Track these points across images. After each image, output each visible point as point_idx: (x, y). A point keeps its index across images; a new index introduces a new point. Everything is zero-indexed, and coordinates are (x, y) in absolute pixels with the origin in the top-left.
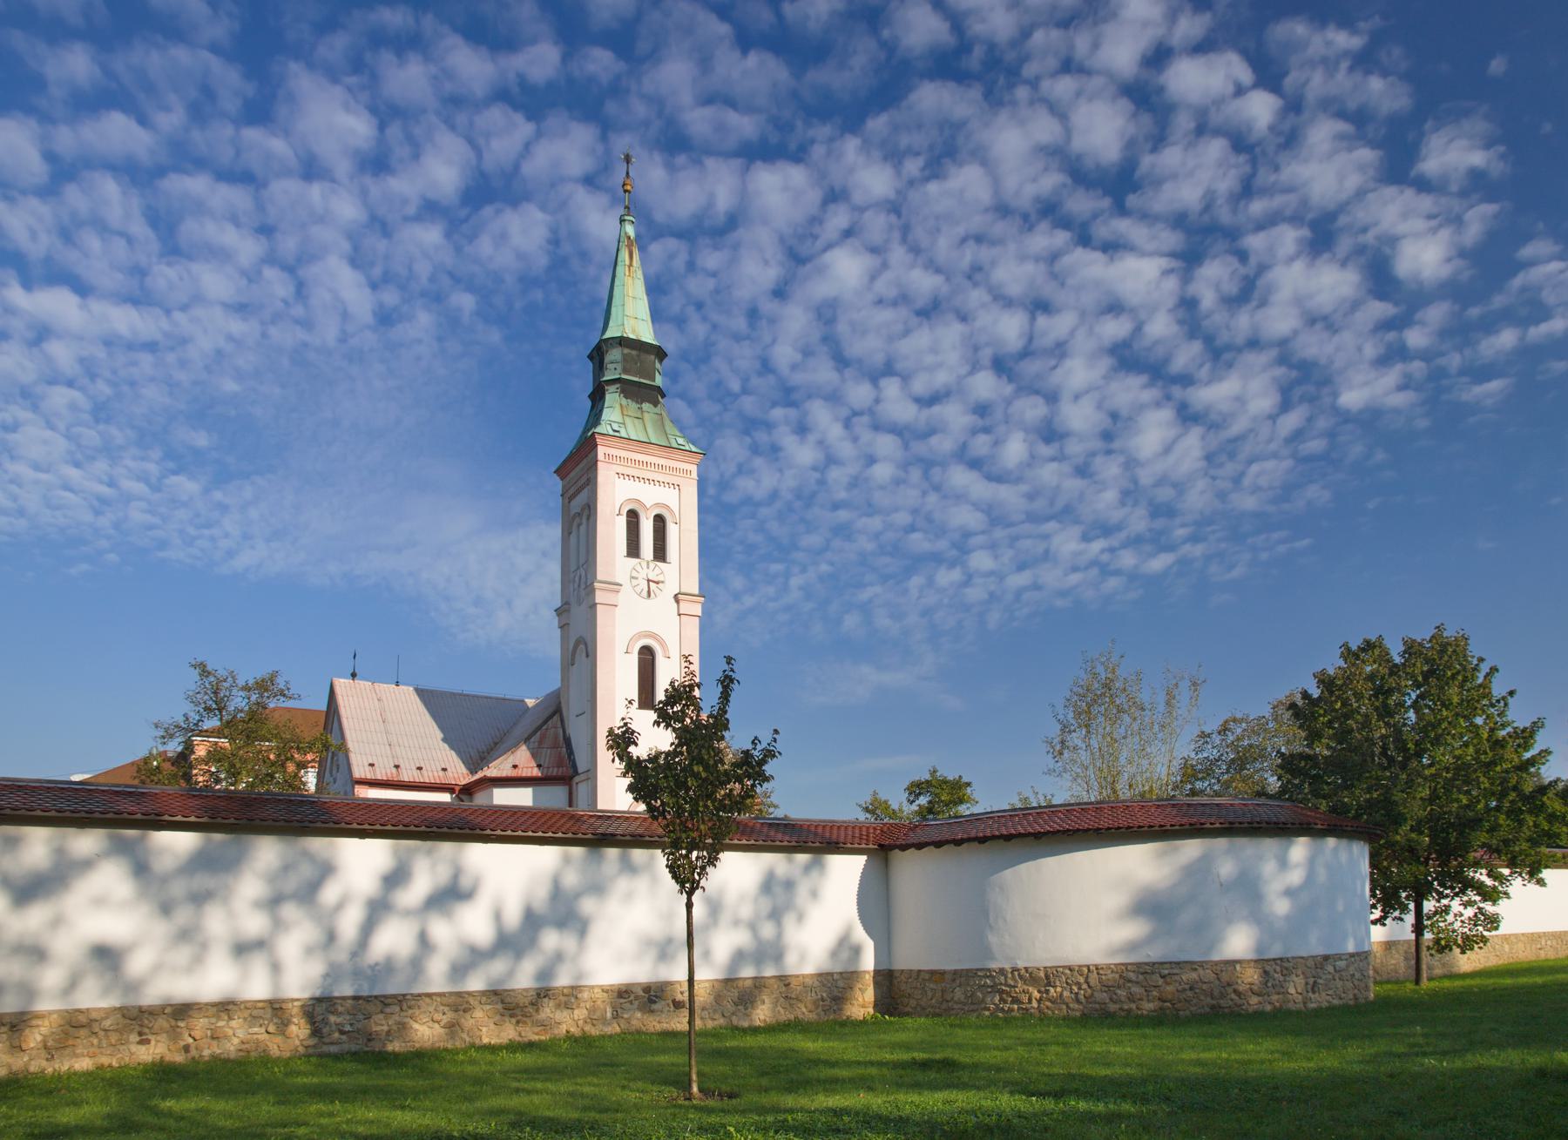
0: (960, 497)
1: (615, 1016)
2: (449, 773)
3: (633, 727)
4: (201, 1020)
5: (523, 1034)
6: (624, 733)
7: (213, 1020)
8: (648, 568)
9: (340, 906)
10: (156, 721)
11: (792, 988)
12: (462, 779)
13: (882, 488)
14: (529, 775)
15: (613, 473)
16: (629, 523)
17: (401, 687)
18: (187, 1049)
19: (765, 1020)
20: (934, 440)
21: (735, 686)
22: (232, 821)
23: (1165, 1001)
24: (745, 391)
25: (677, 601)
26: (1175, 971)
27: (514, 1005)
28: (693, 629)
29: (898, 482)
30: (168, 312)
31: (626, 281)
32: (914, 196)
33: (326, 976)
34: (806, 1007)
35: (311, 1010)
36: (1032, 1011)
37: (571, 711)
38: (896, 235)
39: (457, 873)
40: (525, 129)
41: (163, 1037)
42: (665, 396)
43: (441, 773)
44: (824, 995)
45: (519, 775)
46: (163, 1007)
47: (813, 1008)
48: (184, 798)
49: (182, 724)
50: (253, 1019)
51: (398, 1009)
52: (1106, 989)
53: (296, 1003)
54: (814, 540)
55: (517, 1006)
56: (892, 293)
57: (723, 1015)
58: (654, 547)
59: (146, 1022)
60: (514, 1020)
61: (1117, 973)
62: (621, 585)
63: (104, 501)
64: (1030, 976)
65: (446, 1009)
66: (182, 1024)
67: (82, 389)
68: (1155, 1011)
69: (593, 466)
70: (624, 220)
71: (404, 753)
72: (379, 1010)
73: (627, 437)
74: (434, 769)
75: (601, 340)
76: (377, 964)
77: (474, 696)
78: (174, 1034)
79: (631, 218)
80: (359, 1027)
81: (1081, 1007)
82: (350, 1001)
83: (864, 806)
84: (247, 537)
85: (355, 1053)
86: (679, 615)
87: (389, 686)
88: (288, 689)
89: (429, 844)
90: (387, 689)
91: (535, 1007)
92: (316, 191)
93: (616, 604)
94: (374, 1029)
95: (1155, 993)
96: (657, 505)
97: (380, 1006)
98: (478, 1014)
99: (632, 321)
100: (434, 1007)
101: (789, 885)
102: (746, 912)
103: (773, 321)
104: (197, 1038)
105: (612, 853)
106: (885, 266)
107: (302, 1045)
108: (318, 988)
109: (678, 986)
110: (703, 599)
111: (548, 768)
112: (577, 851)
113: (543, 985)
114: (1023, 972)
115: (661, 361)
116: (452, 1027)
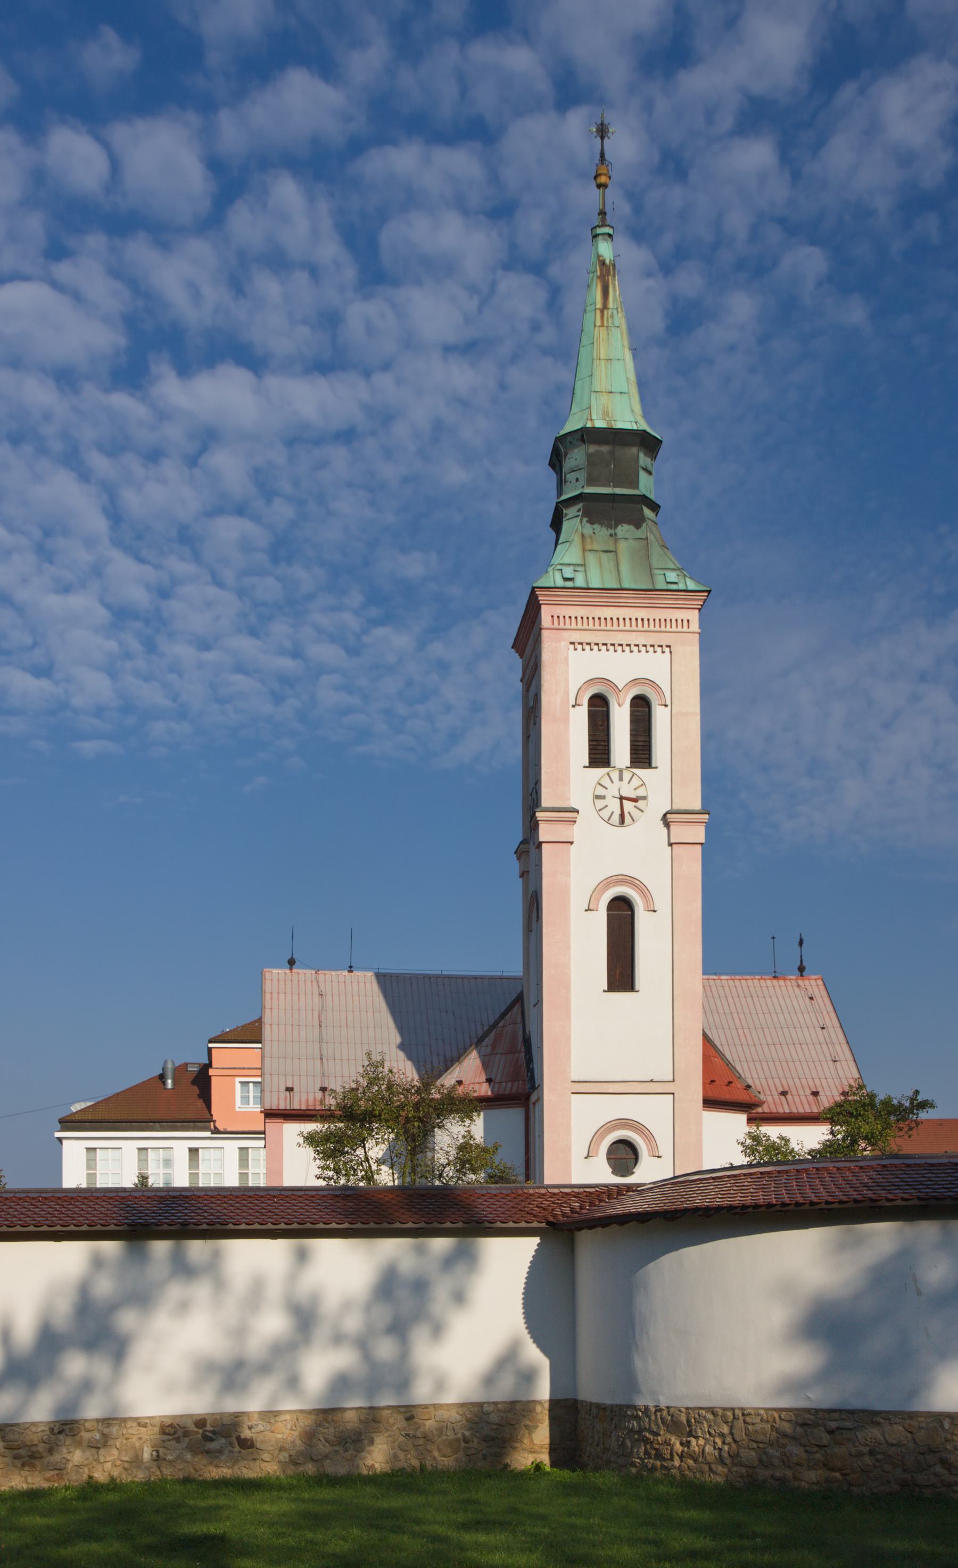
8: (621, 779)
11: (416, 1423)
16: (592, 717)
17: (356, 973)
23: (833, 1470)
25: (667, 824)
26: (848, 1424)
30: (367, 374)
36: (673, 1471)
42: (659, 507)
47: (449, 1452)
52: (755, 1445)
61: (768, 1421)
63: (287, 681)
64: (672, 1420)
67: (257, 519)
68: (818, 1483)
81: (726, 1470)
86: (671, 845)
90: (335, 979)
91: (47, 1446)
95: (818, 1456)
96: (635, 682)
101: (420, 1286)
102: (353, 1323)
105: (161, 1248)
110: (707, 816)
111: (500, 1083)
112: (110, 1248)
113: (70, 1417)
114: (665, 1413)
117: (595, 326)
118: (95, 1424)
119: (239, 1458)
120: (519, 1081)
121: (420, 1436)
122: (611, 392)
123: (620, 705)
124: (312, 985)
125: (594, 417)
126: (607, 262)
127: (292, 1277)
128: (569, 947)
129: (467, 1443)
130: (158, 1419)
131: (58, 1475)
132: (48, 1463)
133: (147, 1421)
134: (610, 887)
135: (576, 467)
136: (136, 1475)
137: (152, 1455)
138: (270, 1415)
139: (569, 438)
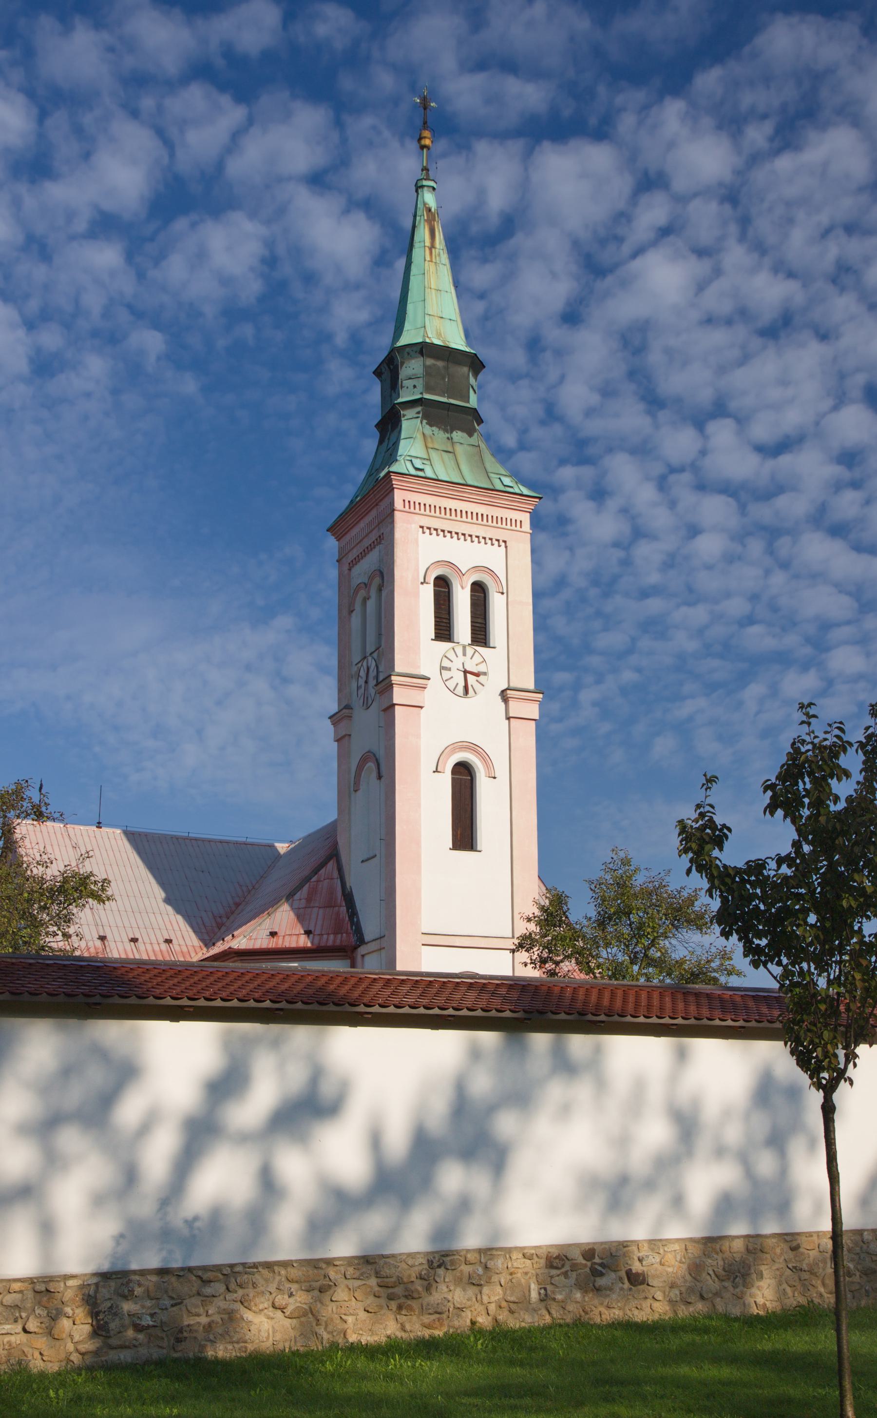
0: (816, 577)
1: (543, 1296)
2: (175, 946)
3: (719, 820)
8: (464, 654)
9: (145, 1129)
11: (802, 1254)
12: (193, 954)
13: (709, 567)
15: (415, 527)
17: (104, 829)
19: (765, 1305)
20: (782, 502)
27: (393, 1280)
29: (730, 559)
31: (427, 268)
32: (760, 176)
34: (824, 1285)
35: (92, 1293)
38: (733, 229)
39: (317, 1074)
43: (164, 946)
45: (280, 946)
53: (70, 1283)
54: (614, 639)
56: (726, 307)
57: (702, 1297)
58: (472, 626)
60: (394, 1305)
62: (429, 679)
65: (294, 1287)
69: (388, 516)
70: (422, 187)
72: (194, 1290)
73: (434, 477)
74: (154, 941)
76: (196, 1218)
79: (432, 184)
80: (164, 1319)
82: (154, 1278)
85: (160, 1363)
87: (87, 828)
88: (47, 804)
89: (275, 1028)
91: (425, 1283)
94: (186, 1323)
97: (197, 1283)
98: (341, 1294)
99: (436, 322)
100: (275, 1285)
102: (733, 1134)
103: (560, 353)
105: (541, 1041)
106: (718, 272)
107: (77, 1350)
109: (634, 1248)
110: (541, 696)
112: (489, 1038)
113: (445, 1247)
115: (476, 375)
117: (425, 260)
118: (477, 1255)
119: (630, 1297)
120: (342, 934)
121: (806, 1269)
123: (463, 588)
124: (63, 837)
126: (433, 210)
128: (419, 805)
130: (545, 1248)
131: (439, 1319)
132: (428, 1305)
133: (533, 1251)
134: (456, 752)
136: (524, 1319)
137: (540, 1294)
138: (654, 1243)
139: (407, 350)
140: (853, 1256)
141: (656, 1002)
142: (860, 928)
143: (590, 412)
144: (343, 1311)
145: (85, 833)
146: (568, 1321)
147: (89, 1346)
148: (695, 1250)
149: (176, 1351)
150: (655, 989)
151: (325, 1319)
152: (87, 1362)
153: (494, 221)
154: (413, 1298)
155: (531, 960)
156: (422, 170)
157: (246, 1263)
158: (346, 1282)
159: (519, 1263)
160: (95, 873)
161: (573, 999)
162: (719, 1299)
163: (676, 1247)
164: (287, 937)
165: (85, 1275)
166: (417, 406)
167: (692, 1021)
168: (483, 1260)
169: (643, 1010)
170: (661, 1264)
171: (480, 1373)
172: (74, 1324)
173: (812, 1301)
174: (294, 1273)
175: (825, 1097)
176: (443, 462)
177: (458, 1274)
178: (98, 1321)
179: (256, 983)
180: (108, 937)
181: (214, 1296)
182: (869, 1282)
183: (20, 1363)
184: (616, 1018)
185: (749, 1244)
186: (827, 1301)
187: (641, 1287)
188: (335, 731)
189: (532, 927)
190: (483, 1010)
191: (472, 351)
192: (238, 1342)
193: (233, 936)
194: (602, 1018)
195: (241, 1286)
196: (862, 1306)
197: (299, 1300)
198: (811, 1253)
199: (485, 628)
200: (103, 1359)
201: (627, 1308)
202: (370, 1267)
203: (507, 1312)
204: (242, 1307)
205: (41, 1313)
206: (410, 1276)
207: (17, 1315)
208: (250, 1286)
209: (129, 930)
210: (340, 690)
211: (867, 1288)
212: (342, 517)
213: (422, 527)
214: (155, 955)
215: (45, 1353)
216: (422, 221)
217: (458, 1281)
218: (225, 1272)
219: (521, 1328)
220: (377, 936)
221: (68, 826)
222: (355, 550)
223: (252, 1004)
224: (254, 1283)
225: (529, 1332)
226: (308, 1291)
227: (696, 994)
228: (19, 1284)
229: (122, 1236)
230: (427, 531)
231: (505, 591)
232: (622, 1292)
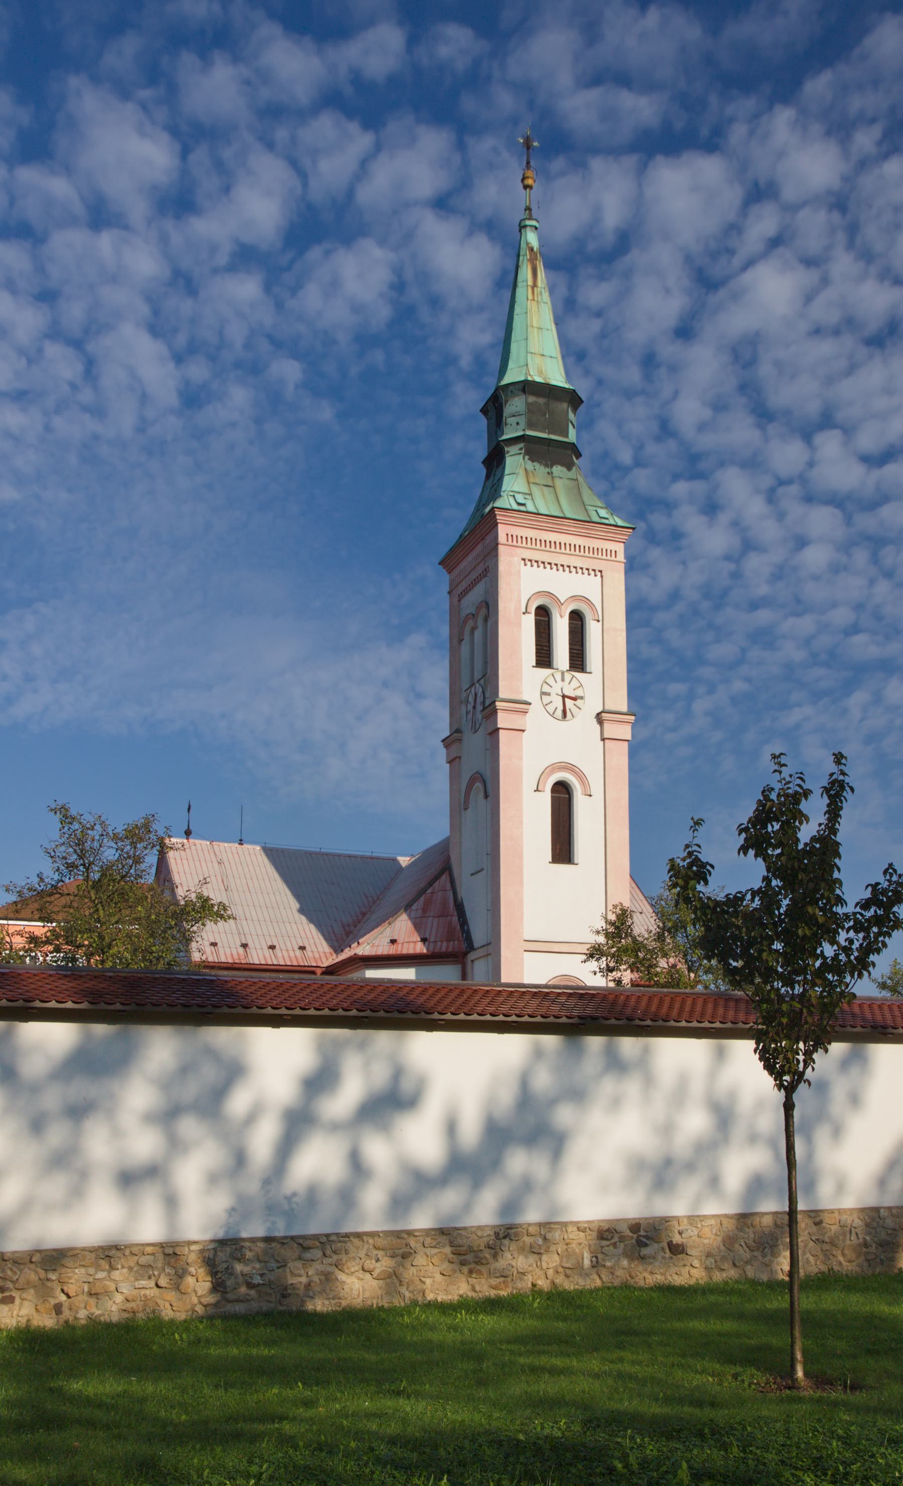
1: (594, 1263)
2: (308, 953)
3: (703, 858)
4: (77, 1271)
5: (478, 1288)
6: (691, 865)
7: (91, 1271)
8: (563, 680)
9: (252, 1118)
10: (7, 883)
11: (825, 1228)
12: (324, 960)
13: (816, 578)
14: (411, 951)
15: (517, 560)
16: (538, 624)
17: (246, 846)
18: (58, 1309)
20: (886, 512)
21: (847, 794)
22: (118, 1006)
24: (638, 463)
27: (464, 1248)
28: (620, 757)
29: (836, 569)
32: (867, 182)
33: (232, 1211)
34: (843, 1255)
35: (211, 1256)
37: (463, 869)
38: (841, 237)
39: (398, 1073)
40: (363, 141)
41: (30, 1294)
42: (581, 455)
43: (298, 953)
44: (868, 1238)
45: (399, 952)
46: (31, 1254)
48: (53, 979)
49: (37, 886)
50: (145, 1270)
51: (320, 1254)
53: (193, 1247)
54: (724, 651)
55: (470, 1250)
56: (833, 317)
57: (734, 1265)
58: (570, 653)
59: (9, 1273)
60: (465, 1270)
62: (530, 704)
65: (380, 1254)
66: (53, 1276)
70: (525, 226)
71: (264, 928)
74: (290, 948)
75: (498, 388)
76: (294, 1194)
77: (334, 855)
78: (43, 1289)
79: (534, 223)
80: (272, 1278)
82: (261, 1245)
83: (880, 980)
84: (29, 678)
85: (267, 1315)
86: (603, 739)
87: (231, 845)
89: (361, 1033)
90: (227, 849)
91: (493, 1251)
92: (106, 241)
93: (523, 729)
94: (290, 1282)
96: (574, 598)
98: (420, 1260)
99: (538, 359)
100: (364, 1252)
103: (674, 368)
104: (71, 1295)
105: (595, 1043)
106: (825, 281)
107: (200, 1303)
108: (221, 1227)
110: (633, 718)
112: (550, 1041)
113: (508, 1221)
116: (393, 1279)
118: (537, 1228)
120: (454, 941)
121: (828, 1241)
122: (543, 355)
123: (561, 616)
125: (532, 373)
126: (535, 249)
127: (712, 1075)
128: (521, 823)
129: (867, 1248)
130: (597, 1222)
131: (504, 1282)
132: (495, 1269)
133: (586, 1225)
135: (516, 412)
137: (592, 1261)
138: (693, 1219)
139: (511, 388)
140: (871, 1230)
141: (699, 1008)
142: (822, 952)
143: (702, 427)
144: (422, 1274)
145: (229, 851)
146: (616, 1284)
147: (211, 1299)
148: (729, 1225)
149: (282, 1305)
150: (688, 995)
151: (407, 1280)
152: (209, 1312)
153: (609, 238)
154: (482, 1264)
155: (600, 968)
156: (526, 210)
157: (339, 1233)
158: (425, 1250)
159: (574, 1235)
160: (211, 897)
161: (625, 1005)
162: (749, 1267)
163: (713, 1222)
164: (405, 944)
165: (205, 1241)
166: (520, 443)
167: (729, 1025)
168: (542, 1233)
169: (685, 1015)
170: (699, 1236)
171: (525, 1324)
172: (197, 1281)
173: (832, 1269)
174: (380, 1242)
175: (786, 1097)
176: (543, 495)
177: (521, 1244)
178: (217, 1279)
179: (346, 994)
180: (249, 945)
181: (313, 1260)
182: (884, 1252)
183: (154, 1312)
184: (660, 1023)
185: (778, 1220)
186: (845, 1268)
187: (681, 1256)
188: (448, 754)
189: (601, 939)
190: (543, 1016)
191: (571, 388)
192: (333, 1299)
193: (358, 943)
194: (648, 1022)
195: (335, 1252)
196: (877, 1272)
197: (384, 1264)
198: (833, 1227)
199: (583, 654)
200: (222, 1310)
201: (668, 1274)
202: (445, 1237)
203: (563, 1277)
204: (336, 1269)
205: (170, 1272)
206: (479, 1246)
207: (151, 1273)
208: (343, 1252)
209: (268, 939)
210: (451, 715)
211: (882, 1257)
212: (452, 551)
213: (524, 560)
214: (291, 961)
215: (174, 1304)
216: (525, 261)
217: (522, 1250)
218: (322, 1241)
219: (575, 1290)
220: (485, 943)
221: (214, 843)
222: (463, 583)
223: (340, 1012)
224: (346, 1250)
225: (580, 1293)
226: (392, 1257)
227: (736, 1000)
228: (151, 1248)
229: (233, 1209)
230: (529, 563)
231: (600, 619)
232: (663, 1261)
